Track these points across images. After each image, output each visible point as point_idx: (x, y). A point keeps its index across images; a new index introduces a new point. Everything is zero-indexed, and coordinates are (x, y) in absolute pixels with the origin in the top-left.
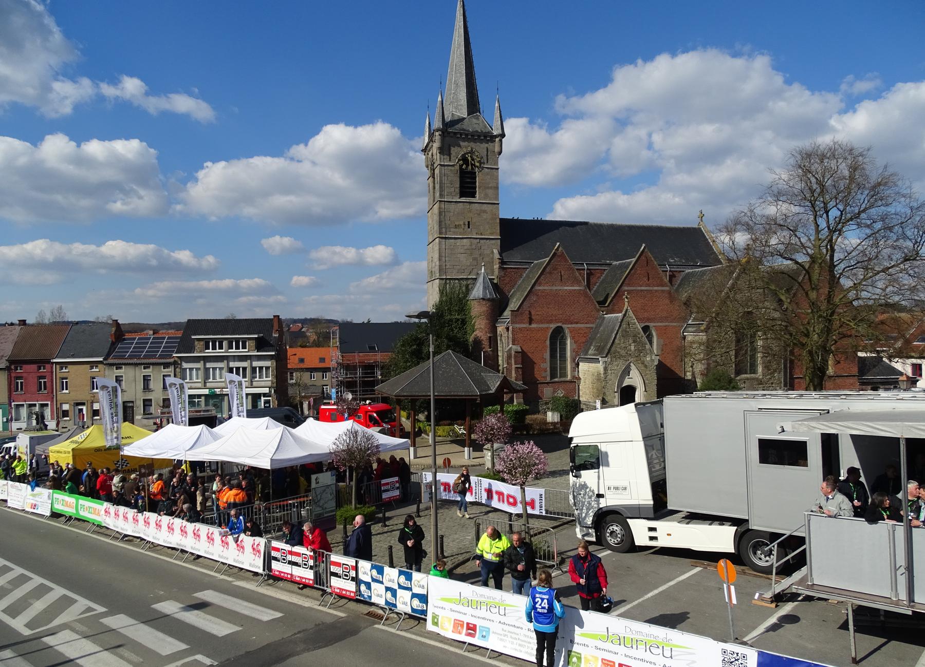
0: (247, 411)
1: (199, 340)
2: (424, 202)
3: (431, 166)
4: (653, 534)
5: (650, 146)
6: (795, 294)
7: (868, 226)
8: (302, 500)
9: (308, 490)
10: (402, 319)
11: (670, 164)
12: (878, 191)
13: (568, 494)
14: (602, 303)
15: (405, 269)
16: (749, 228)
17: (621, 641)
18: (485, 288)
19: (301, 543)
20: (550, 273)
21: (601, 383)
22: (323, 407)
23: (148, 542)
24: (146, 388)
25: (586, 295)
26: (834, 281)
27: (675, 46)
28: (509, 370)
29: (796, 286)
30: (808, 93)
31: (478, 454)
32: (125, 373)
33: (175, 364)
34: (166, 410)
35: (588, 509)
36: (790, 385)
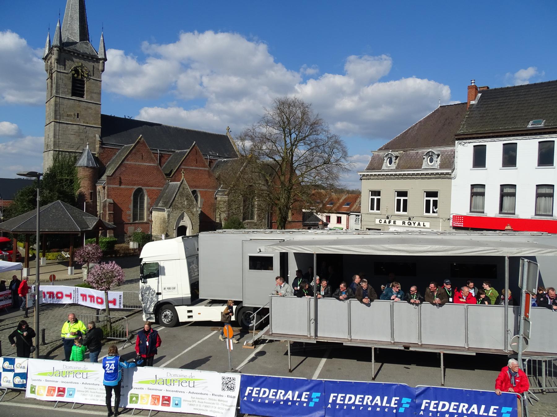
2: (43, 95)
3: (50, 71)
4: (190, 314)
5: (201, 84)
6: (274, 178)
7: (309, 144)
10: (15, 176)
11: (213, 96)
12: (314, 126)
13: (138, 294)
14: (168, 175)
15: (28, 141)
16: (252, 139)
17: (164, 382)
18: (88, 160)
20: (135, 154)
21: (166, 223)
25: (158, 169)
26: (292, 171)
27: (218, 27)
28: (104, 215)
29: (275, 173)
30: (285, 69)
31: (78, 271)
35: (151, 302)
36: (270, 226)
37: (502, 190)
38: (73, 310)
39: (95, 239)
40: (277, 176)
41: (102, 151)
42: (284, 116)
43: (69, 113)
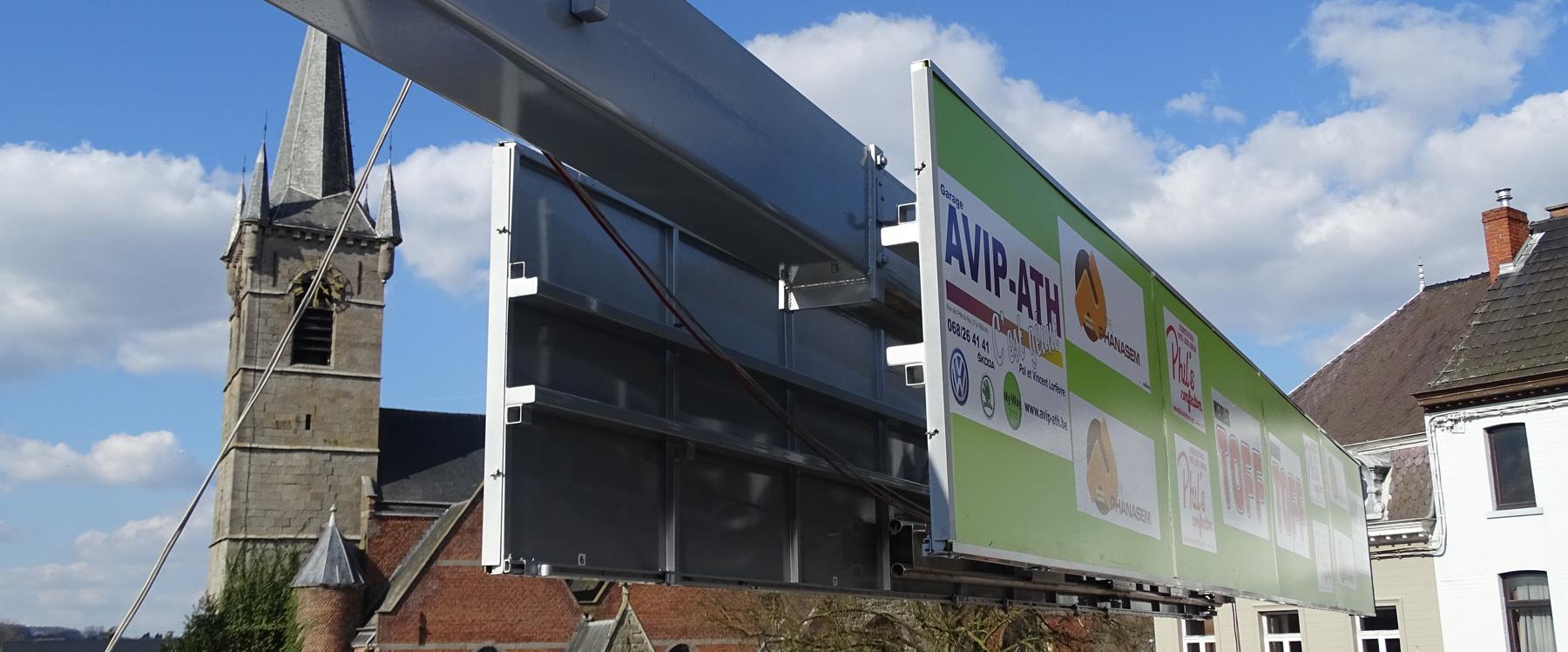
18: (331, 562)
37: (1509, 593)
41: (377, 529)
43: (281, 418)
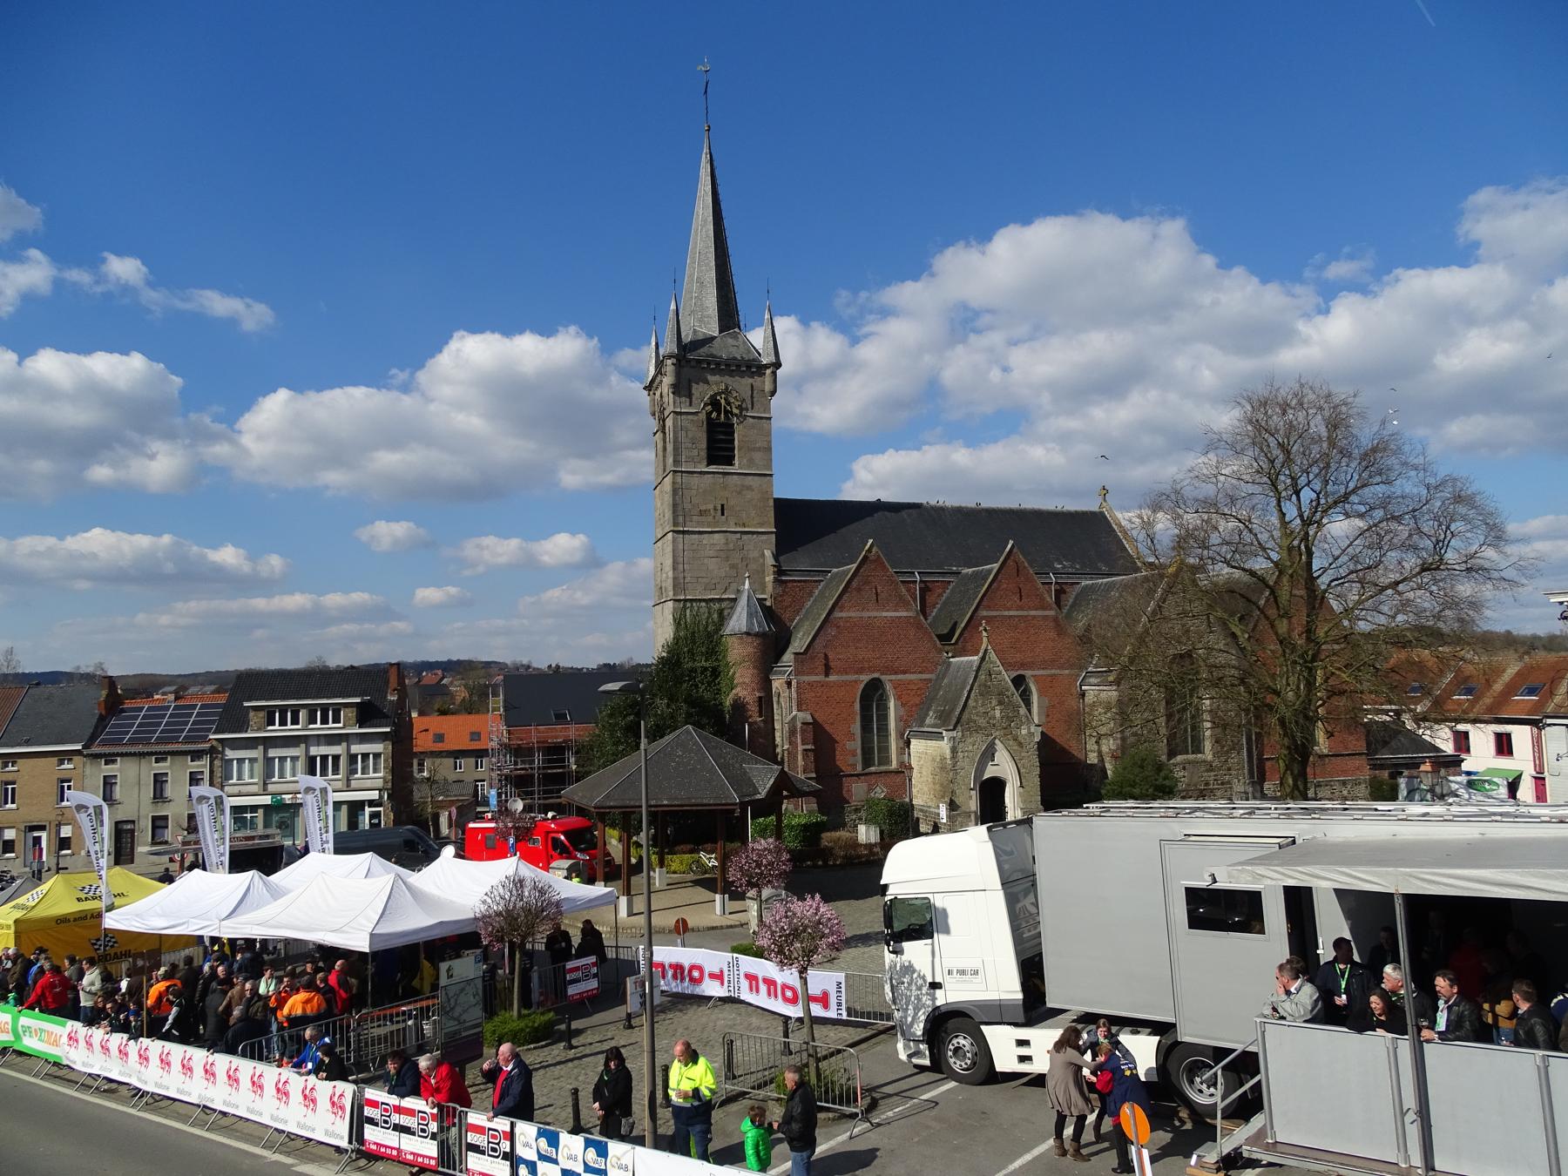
0: (336, 836)
1: (256, 708)
4: (1024, 1051)
7: (1361, 516)
8: (424, 1004)
9: (435, 987)
12: (1374, 460)
14: (945, 638)
18: (750, 615)
19: (415, 1092)
20: (859, 590)
21: (948, 771)
22: (471, 825)
23: (145, 1093)
24: (159, 796)
25: (919, 626)
28: (792, 754)
31: (737, 905)
32: (120, 770)
33: (212, 752)
34: (192, 837)
35: (917, 1009)
38: (728, 1014)
39: (773, 817)
40: (1264, 622)
41: (780, 590)
42: (1273, 443)
43: (703, 508)
